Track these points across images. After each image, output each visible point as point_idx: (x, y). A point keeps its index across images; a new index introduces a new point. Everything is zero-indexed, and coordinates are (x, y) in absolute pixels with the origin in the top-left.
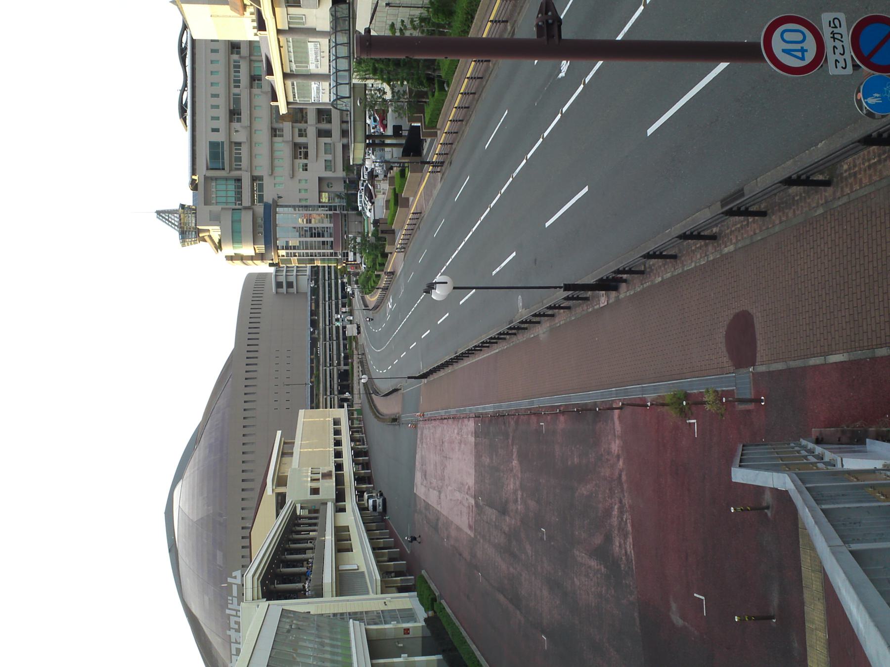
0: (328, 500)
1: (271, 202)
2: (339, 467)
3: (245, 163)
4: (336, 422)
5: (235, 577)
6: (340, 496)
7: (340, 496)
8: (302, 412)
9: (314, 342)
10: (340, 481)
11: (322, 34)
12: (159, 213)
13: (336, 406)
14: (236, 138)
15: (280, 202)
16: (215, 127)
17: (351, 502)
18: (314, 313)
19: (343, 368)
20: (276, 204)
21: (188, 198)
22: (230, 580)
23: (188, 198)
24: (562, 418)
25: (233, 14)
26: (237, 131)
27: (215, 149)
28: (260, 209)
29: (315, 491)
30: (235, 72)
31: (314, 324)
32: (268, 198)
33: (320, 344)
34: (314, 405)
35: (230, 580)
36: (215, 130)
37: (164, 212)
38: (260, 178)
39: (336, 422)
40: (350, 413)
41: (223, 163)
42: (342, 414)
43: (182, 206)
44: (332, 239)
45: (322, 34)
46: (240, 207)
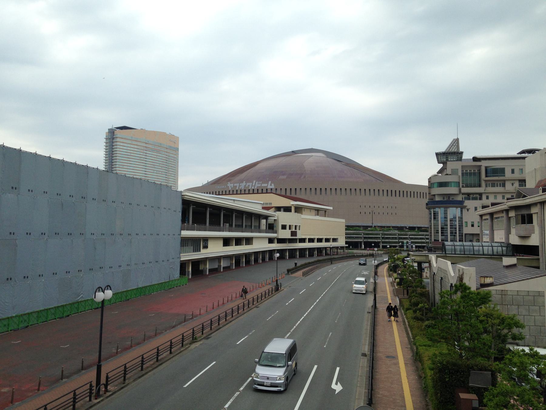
0: (278, 235)
1: (465, 204)
2: (302, 240)
3: (490, 189)
4: (335, 240)
5: (271, 185)
6: (280, 241)
7: (280, 241)
8: (344, 221)
9: (400, 229)
10: (291, 241)
11: (507, 238)
12: (457, 140)
13: (347, 240)
14: (508, 185)
15: (465, 211)
16: (515, 171)
17: (275, 246)
18: (420, 229)
19: (381, 245)
20: (462, 208)
21: (467, 156)
22: (270, 182)
23: (467, 156)
24: (109, 387)
25: (537, 182)
26: (513, 184)
27: (501, 171)
28: (460, 198)
29: (284, 227)
30: (500, 184)
31: (412, 229)
32: (467, 203)
33: (396, 232)
34: (348, 227)
35: (270, 182)
36: (513, 171)
37: (458, 143)
38: (481, 199)
39: (335, 240)
40: (342, 248)
41: (491, 176)
42: (342, 242)
43: (462, 153)
44: (440, 241)
45: (507, 238)
46: (461, 186)
